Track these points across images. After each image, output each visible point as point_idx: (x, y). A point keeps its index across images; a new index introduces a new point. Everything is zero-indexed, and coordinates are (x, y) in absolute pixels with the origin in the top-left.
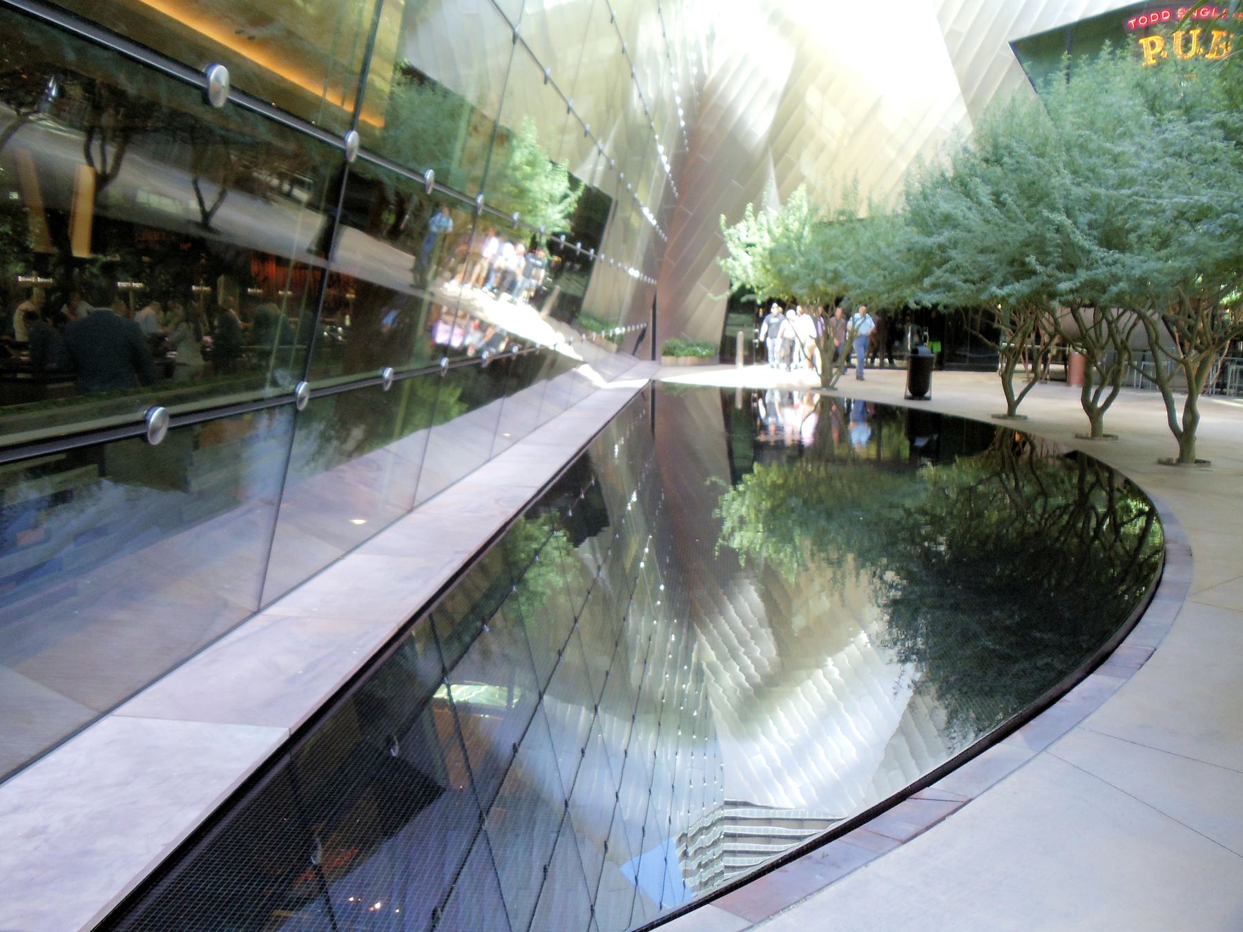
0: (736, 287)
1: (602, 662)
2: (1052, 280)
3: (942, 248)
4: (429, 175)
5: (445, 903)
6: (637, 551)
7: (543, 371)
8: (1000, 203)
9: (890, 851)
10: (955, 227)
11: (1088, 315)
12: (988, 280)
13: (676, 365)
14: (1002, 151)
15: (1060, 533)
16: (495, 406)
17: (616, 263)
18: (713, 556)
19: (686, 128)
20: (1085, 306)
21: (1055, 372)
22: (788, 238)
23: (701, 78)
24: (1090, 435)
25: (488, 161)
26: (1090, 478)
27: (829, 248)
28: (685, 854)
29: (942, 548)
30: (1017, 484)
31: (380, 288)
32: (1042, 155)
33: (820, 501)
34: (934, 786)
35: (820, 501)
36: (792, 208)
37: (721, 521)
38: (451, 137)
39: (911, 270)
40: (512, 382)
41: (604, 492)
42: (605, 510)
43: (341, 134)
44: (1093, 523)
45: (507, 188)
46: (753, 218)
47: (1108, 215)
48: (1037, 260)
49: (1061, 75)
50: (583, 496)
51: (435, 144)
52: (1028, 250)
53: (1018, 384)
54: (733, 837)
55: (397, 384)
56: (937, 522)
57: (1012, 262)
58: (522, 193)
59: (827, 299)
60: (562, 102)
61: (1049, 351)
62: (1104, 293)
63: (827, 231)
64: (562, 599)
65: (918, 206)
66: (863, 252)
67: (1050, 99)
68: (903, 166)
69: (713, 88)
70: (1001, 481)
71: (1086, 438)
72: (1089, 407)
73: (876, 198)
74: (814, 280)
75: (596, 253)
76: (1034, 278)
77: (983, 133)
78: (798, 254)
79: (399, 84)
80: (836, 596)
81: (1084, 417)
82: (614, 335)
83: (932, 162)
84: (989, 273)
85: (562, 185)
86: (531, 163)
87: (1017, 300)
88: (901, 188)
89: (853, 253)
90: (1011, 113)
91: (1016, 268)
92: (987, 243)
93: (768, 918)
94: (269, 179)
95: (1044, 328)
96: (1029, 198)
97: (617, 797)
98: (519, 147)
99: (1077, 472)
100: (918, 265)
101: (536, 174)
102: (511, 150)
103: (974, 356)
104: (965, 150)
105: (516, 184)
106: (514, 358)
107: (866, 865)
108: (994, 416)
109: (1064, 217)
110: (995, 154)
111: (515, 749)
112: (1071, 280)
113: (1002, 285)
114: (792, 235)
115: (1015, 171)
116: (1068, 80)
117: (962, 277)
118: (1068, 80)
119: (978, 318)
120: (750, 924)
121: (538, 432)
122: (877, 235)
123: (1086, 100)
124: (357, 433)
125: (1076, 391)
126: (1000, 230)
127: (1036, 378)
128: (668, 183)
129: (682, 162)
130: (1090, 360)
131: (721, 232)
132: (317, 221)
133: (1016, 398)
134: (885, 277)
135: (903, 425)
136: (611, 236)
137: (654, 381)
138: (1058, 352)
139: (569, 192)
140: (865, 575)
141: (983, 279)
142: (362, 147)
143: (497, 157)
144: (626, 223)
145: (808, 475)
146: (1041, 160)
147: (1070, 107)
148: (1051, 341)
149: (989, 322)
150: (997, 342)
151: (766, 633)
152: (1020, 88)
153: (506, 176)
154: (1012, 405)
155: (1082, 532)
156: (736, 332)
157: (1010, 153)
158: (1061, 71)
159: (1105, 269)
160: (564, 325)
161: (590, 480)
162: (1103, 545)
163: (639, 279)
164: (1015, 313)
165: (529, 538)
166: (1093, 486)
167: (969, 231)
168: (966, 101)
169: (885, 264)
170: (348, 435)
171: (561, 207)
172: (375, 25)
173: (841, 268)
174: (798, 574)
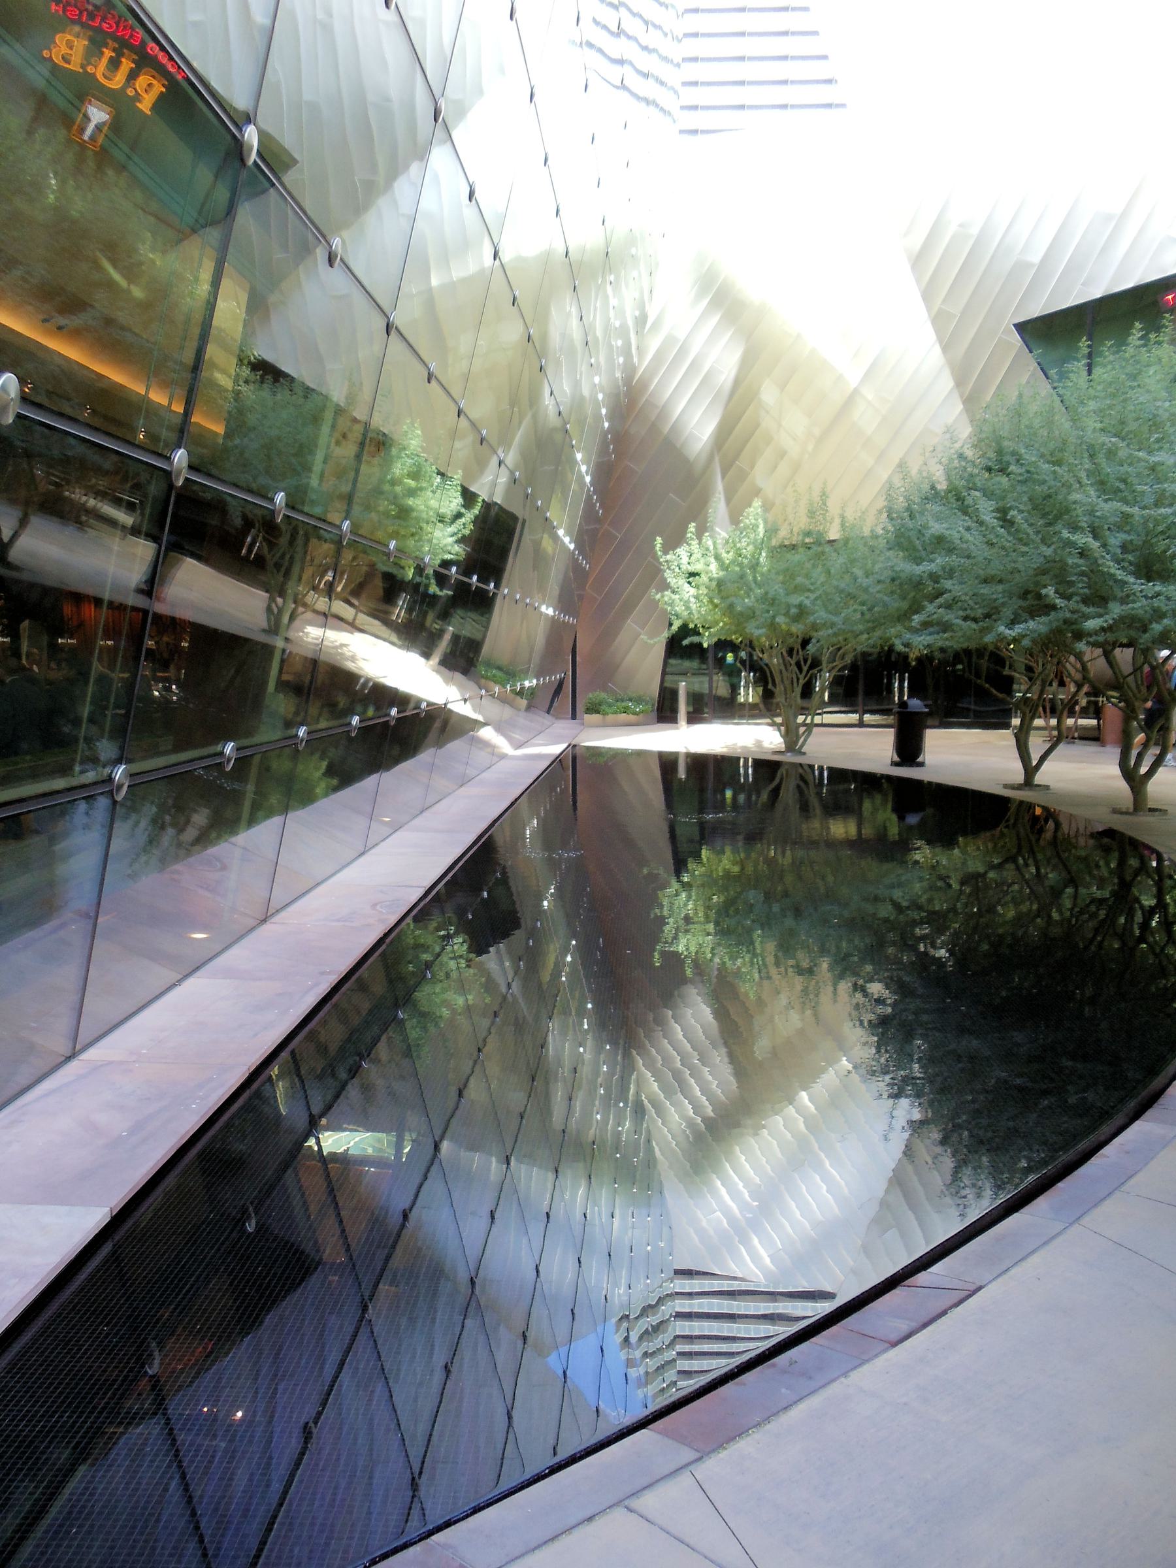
0: (675, 628)
1: (516, 1098)
2: (1076, 616)
3: (934, 578)
4: (280, 498)
5: (329, 1394)
6: (557, 958)
7: (433, 735)
8: (1007, 523)
9: (876, 1356)
10: (951, 551)
11: (1124, 656)
12: (994, 617)
13: (605, 725)
14: (1007, 458)
15: (1097, 931)
16: (370, 782)
17: (523, 598)
18: (652, 964)
19: (609, 430)
20: (1122, 645)
21: (1085, 728)
22: (741, 565)
23: (629, 369)
24: (1131, 810)
25: (357, 471)
26: (1134, 862)
27: (793, 577)
28: (626, 1339)
29: (942, 953)
30: (1038, 869)
31: (224, 634)
32: (1058, 463)
33: (786, 894)
34: (934, 1269)
35: (786, 894)
36: (746, 528)
37: (661, 921)
38: (304, 450)
39: (896, 605)
40: (396, 751)
41: (512, 883)
42: (515, 912)
43: (167, 453)
44: (1139, 917)
45: (383, 505)
46: (697, 541)
47: (1147, 535)
48: (1056, 592)
49: (1080, 365)
50: (485, 894)
51: (295, 455)
52: (1045, 579)
53: (1037, 745)
54: (689, 1316)
55: (242, 762)
56: (937, 921)
57: (1025, 594)
58: (404, 513)
59: (791, 641)
60: (452, 405)
61: (1076, 703)
62: (1145, 631)
63: (789, 556)
64: (462, 1020)
65: (903, 525)
66: (835, 583)
67: (1067, 394)
68: (884, 474)
69: (644, 384)
70: (1018, 868)
71: (1127, 813)
72: (1129, 774)
73: (850, 515)
74: (774, 617)
75: (497, 586)
76: (1053, 613)
77: (983, 436)
78: (753, 585)
79: (246, 382)
80: (809, 1012)
81: (1122, 786)
82: (522, 688)
83: (920, 472)
84: (996, 608)
85: (454, 502)
86: (416, 475)
87: (1034, 641)
88: (881, 503)
89: (823, 584)
90: (1018, 413)
91: (1031, 601)
92: (991, 571)
93: (721, 1446)
94: (84, 498)
95: (1069, 675)
96: (1044, 515)
97: (538, 1272)
98: (400, 457)
99: (1116, 854)
100: (904, 598)
101: (421, 489)
102: (388, 463)
103: (978, 708)
104: (961, 456)
105: (395, 500)
106: (393, 723)
107: (845, 1374)
108: (1006, 786)
109: (1090, 540)
110: (1000, 461)
111: (405, 1216)
112: (1100, 616)
113: (1012, 623)
114: (746, 561)
115: (1024, 482)
116: (1090, 372)
117: (961, 613)
118: (1090, 372)
119: (984, 663)
120: (698, 1455)
121: (426, 814)
122: (853, 561)
123: (1113, 396)
124: (200, 818)
125: (1114, 752)
126: (1007, 556)
127: (1060, 737)
128: (589, 498)
129: (605, 472)
130: (1129, 714)
131: (657, 559)
132: (145, 550)
133: (1034, 763)
134: (863, 614)
135: (890, 798)
136: (516, 567)
137: (575, 746)
138: (1088, 702)
139: (463, 510)
140: (844, 986)
141: (987, 616)
142: (191, 467)
143: (370, 471)
144: (537, 545)
145: (771, 862)
146: (1057, 468)
147: (1092, 405)
148: (1078, 691)
149: (999, 668)
150: (1009, 692)
151: (719, 1057)
152: (1028, 382)
153: (382, 493)
154: (1030, 771)
155: (1124, 929)
156: (677, 682)
157: (1018, 461)
158: (1079, 361)
159: (1144, 602)
160: (458, 676)
161: (495, 872)
162: (1150, 946)
163: (553, 617)
164: (1031, 655)
165: (420, 947)
166: (1137, 872)
167: (968, 557)
168: (961, 397)
169: (864, 597)
170: (188, 822)
171: (451, 529)
172: (211, 306)
173: (807, 602)
174: (760, 985)
